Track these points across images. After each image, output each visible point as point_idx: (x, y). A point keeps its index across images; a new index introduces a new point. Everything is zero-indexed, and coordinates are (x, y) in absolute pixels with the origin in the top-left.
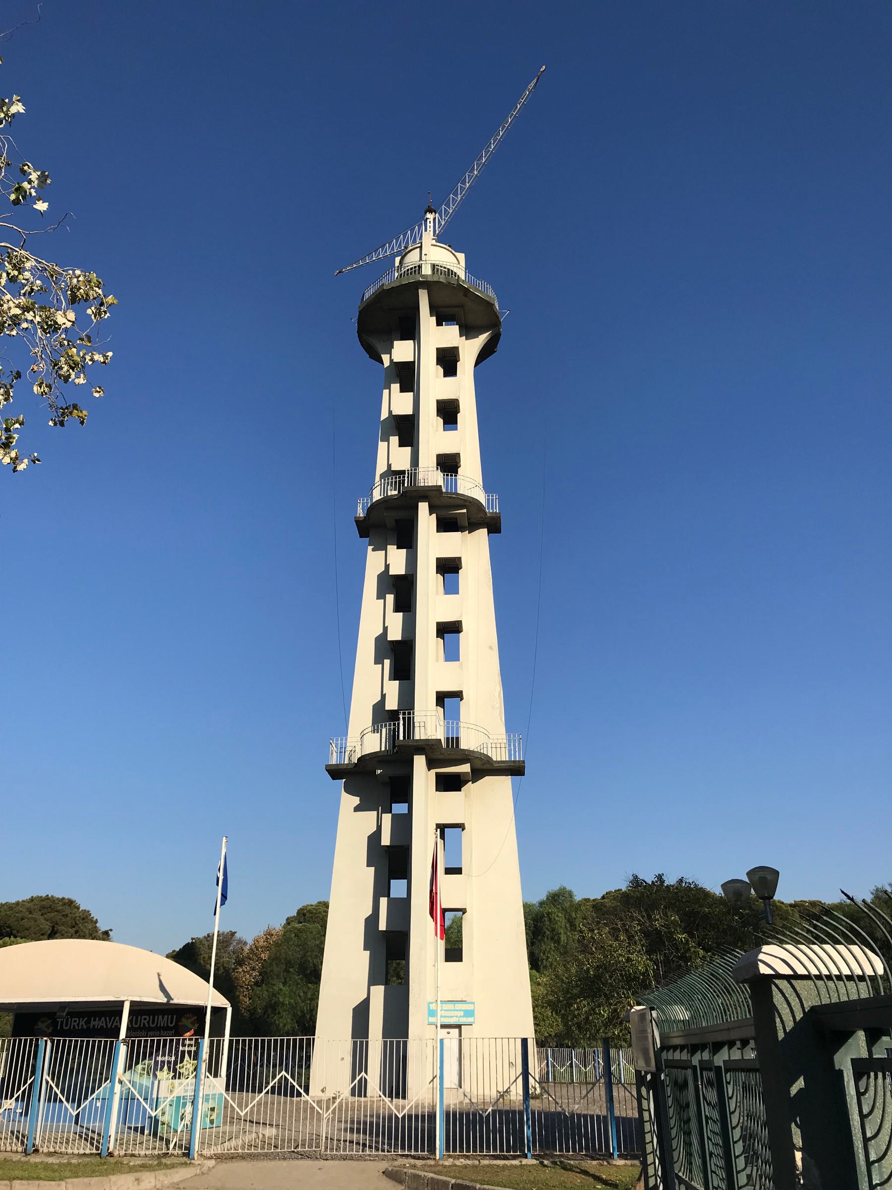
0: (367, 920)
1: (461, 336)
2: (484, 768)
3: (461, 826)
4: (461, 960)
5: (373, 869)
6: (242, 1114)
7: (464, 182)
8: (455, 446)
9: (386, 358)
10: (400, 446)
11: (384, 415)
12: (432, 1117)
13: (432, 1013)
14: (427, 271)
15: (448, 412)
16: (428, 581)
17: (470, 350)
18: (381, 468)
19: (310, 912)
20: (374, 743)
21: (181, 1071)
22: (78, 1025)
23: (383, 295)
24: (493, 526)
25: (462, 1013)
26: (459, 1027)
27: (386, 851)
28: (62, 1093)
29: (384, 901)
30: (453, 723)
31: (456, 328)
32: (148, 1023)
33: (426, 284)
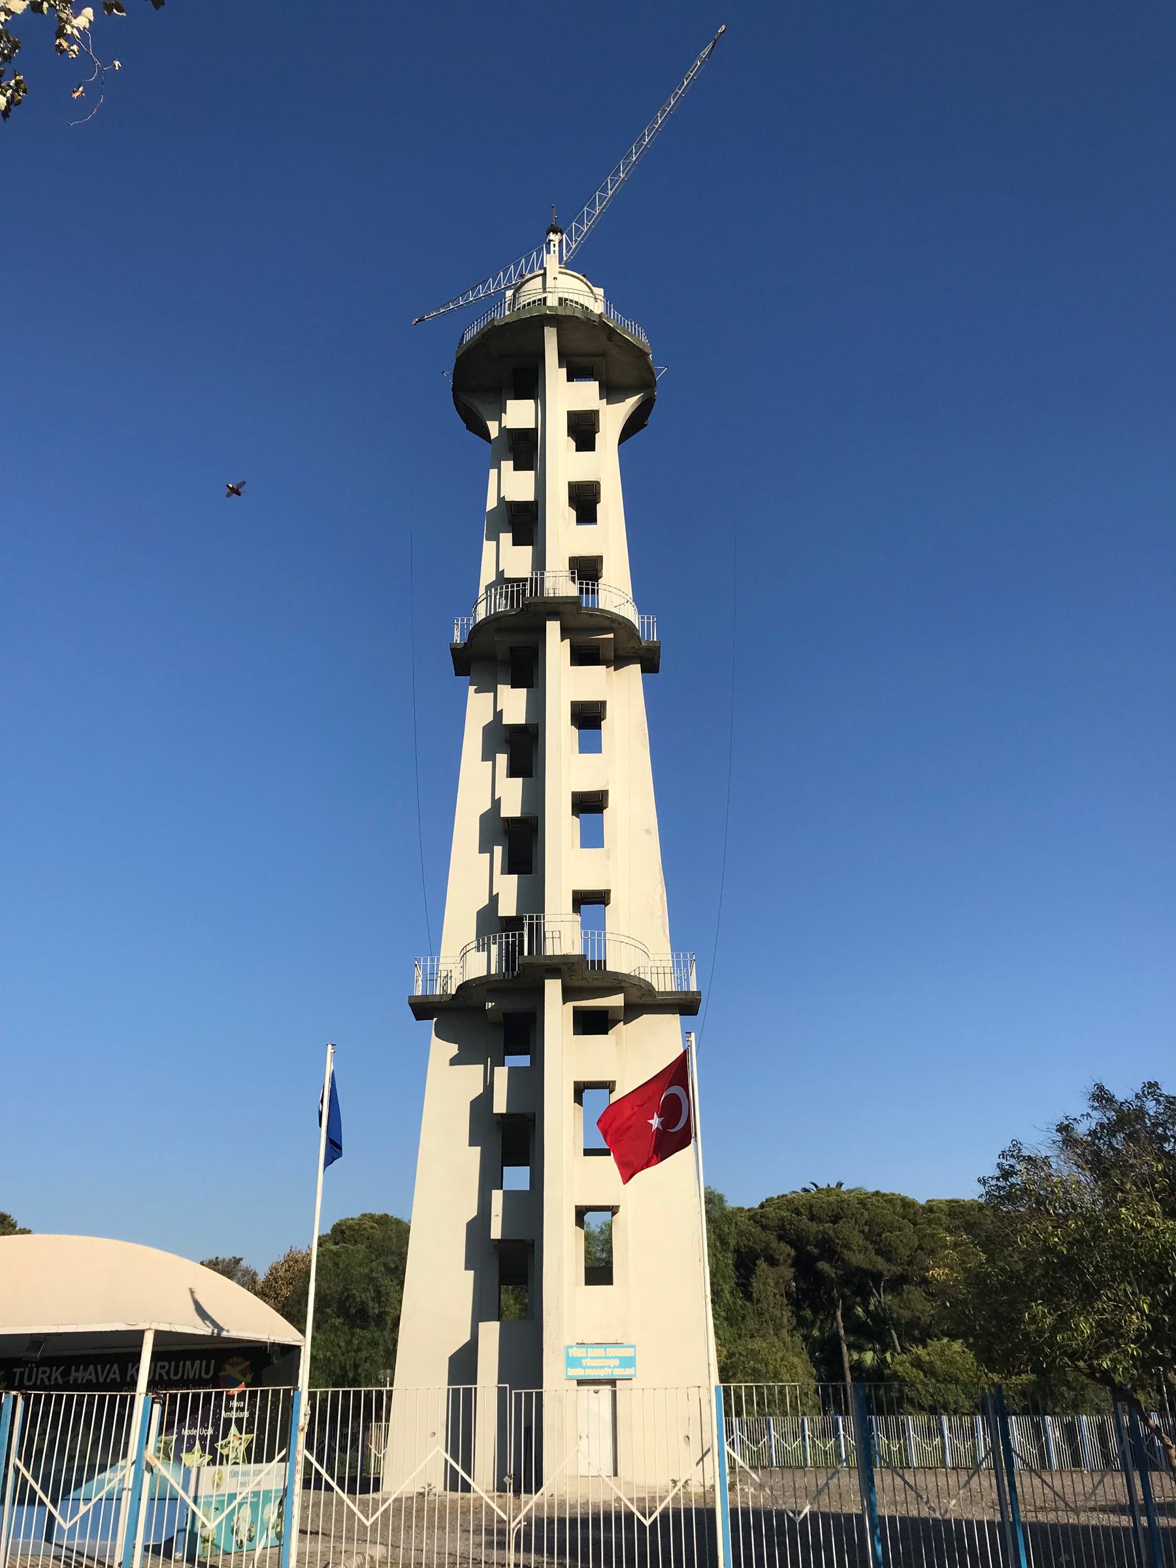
0: (471, 1225)
2: (643, 1001)
5: (477, 1150)
7: (605, 190)
9: (493, 428)
10: (514, 544)
11: (491, 503)
12: (707, 1516)
13: (572, 1362)
14: (552, 301)
16: (560, 733)
17: (613, 418)
18: (487, 575)
19: (350, 1228)
21: (225, 1452)
22: (49, 1378)
23: (494, 333)
24: (650, 663)
25: (617, 1362)
26: (612, 1382)
27: (498, 1123)
28: (45, 1489)
29: (497, 1196)
30: (593, 934)
32: (168, 1373)
33: (554, 320)
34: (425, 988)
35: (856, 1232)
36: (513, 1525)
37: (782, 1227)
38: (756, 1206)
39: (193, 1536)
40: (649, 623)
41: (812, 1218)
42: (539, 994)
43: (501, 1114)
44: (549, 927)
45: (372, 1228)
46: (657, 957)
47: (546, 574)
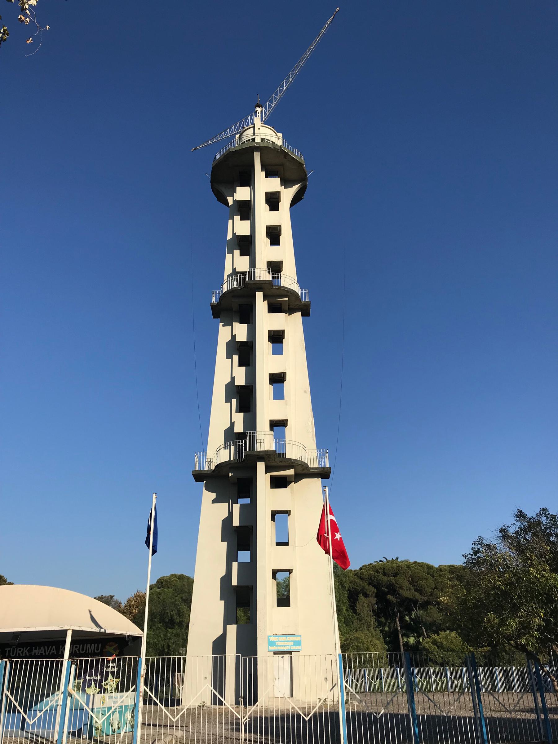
0: (222, 579)
1: (281, 186)
2: (303, 472)
3: (288, 513)
4: (289, 606)
5: (225, 543)
6: (174, 720)
7: (282, 86)
8: (280, 257)
9: (230, 200)
10: (240, 256)
11: (230, 236)
12: (335, 716)
13: (271, 643)
14: (258, 140)
15: (274, 235)
16: (263, 345)
17: (287, 195)
18: (228, 270)
19: (166, 581)
20: (225, 456)
21: (106, 687)
22: (22, 653)
23: (230, 155)
26: (290, 653)
29: (235, 565)
30: (279, 441)
31: (278, 180)
32: (79, 650)
34: (200, 467)
35: (405, 581)
36: (243, 721)
37: (371, 579)
38: (358, 569)
39: (91, 727)
40: (305, 293)
41: (385, 574)
42: (254, 297)
43: (237, 527)
44: (258, 437)
45: (176, 581)
46: (310, 451)
47: (256, 270)
